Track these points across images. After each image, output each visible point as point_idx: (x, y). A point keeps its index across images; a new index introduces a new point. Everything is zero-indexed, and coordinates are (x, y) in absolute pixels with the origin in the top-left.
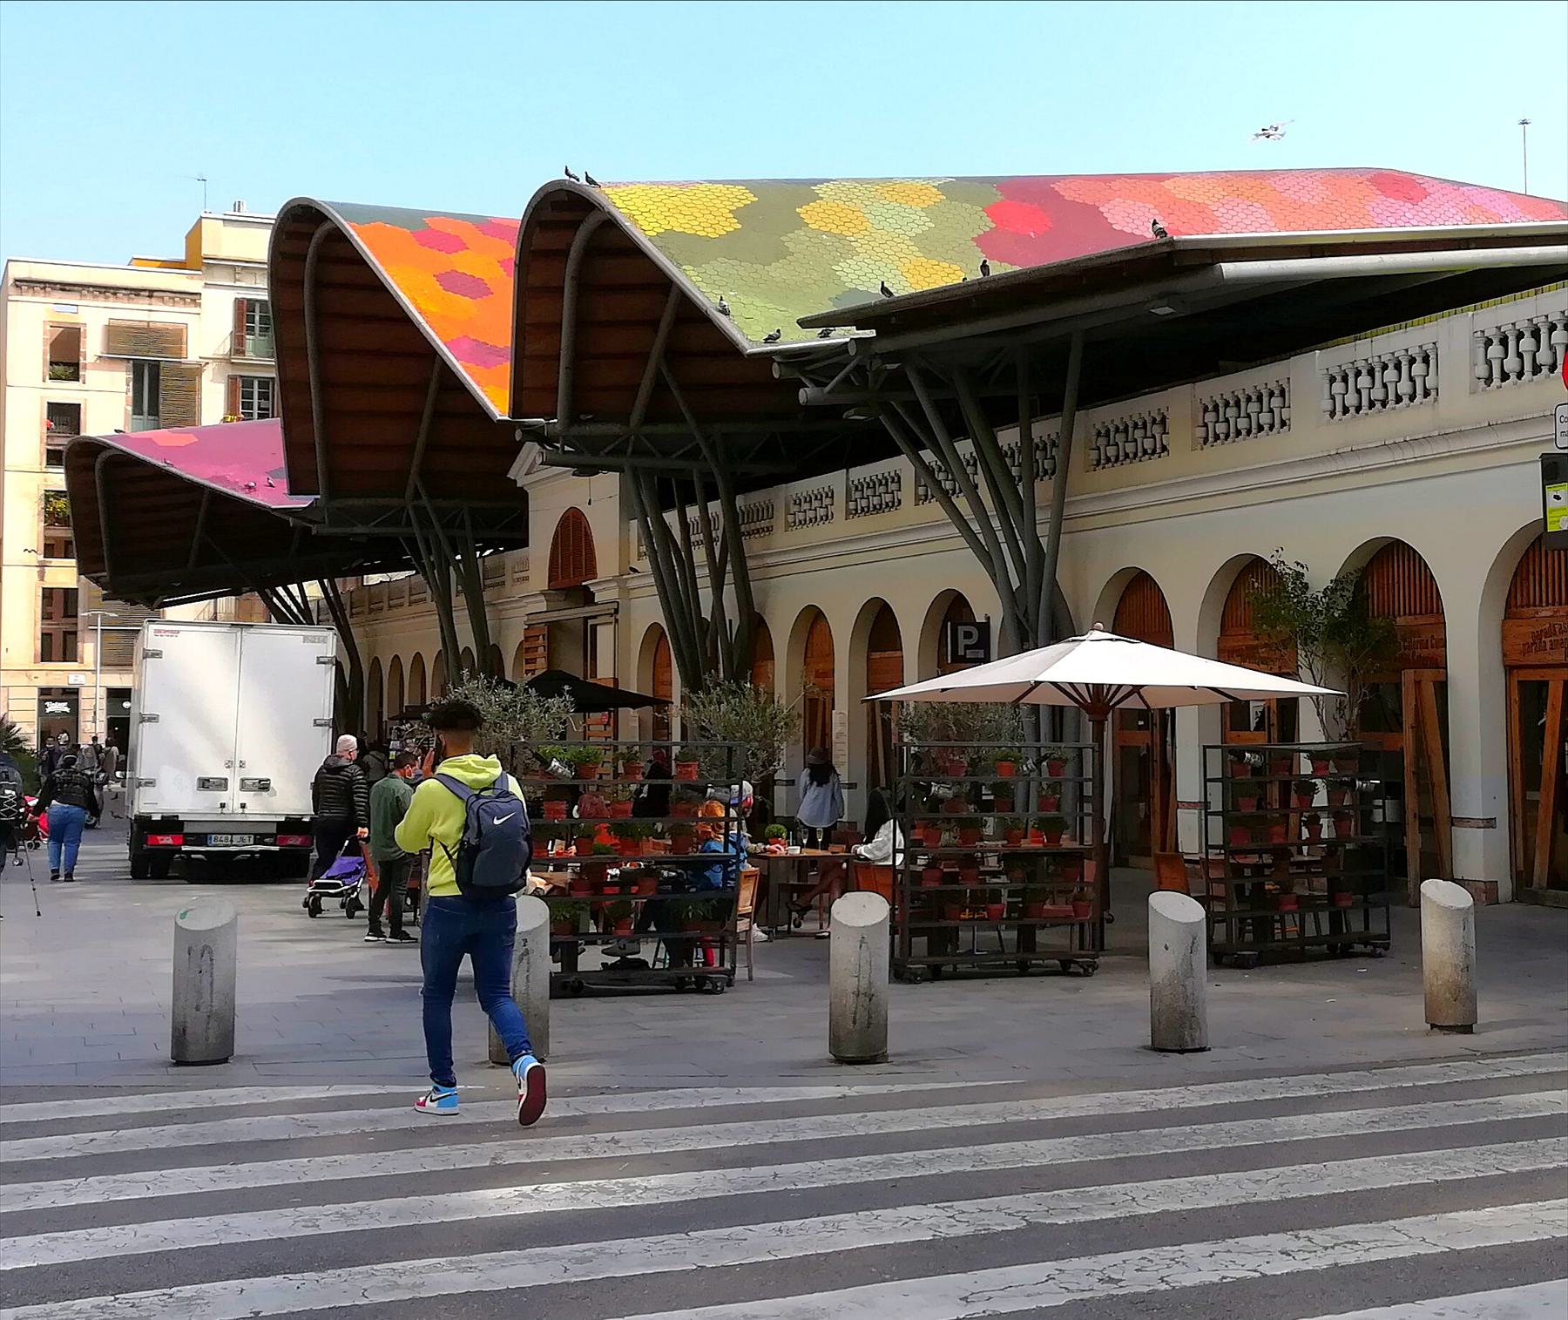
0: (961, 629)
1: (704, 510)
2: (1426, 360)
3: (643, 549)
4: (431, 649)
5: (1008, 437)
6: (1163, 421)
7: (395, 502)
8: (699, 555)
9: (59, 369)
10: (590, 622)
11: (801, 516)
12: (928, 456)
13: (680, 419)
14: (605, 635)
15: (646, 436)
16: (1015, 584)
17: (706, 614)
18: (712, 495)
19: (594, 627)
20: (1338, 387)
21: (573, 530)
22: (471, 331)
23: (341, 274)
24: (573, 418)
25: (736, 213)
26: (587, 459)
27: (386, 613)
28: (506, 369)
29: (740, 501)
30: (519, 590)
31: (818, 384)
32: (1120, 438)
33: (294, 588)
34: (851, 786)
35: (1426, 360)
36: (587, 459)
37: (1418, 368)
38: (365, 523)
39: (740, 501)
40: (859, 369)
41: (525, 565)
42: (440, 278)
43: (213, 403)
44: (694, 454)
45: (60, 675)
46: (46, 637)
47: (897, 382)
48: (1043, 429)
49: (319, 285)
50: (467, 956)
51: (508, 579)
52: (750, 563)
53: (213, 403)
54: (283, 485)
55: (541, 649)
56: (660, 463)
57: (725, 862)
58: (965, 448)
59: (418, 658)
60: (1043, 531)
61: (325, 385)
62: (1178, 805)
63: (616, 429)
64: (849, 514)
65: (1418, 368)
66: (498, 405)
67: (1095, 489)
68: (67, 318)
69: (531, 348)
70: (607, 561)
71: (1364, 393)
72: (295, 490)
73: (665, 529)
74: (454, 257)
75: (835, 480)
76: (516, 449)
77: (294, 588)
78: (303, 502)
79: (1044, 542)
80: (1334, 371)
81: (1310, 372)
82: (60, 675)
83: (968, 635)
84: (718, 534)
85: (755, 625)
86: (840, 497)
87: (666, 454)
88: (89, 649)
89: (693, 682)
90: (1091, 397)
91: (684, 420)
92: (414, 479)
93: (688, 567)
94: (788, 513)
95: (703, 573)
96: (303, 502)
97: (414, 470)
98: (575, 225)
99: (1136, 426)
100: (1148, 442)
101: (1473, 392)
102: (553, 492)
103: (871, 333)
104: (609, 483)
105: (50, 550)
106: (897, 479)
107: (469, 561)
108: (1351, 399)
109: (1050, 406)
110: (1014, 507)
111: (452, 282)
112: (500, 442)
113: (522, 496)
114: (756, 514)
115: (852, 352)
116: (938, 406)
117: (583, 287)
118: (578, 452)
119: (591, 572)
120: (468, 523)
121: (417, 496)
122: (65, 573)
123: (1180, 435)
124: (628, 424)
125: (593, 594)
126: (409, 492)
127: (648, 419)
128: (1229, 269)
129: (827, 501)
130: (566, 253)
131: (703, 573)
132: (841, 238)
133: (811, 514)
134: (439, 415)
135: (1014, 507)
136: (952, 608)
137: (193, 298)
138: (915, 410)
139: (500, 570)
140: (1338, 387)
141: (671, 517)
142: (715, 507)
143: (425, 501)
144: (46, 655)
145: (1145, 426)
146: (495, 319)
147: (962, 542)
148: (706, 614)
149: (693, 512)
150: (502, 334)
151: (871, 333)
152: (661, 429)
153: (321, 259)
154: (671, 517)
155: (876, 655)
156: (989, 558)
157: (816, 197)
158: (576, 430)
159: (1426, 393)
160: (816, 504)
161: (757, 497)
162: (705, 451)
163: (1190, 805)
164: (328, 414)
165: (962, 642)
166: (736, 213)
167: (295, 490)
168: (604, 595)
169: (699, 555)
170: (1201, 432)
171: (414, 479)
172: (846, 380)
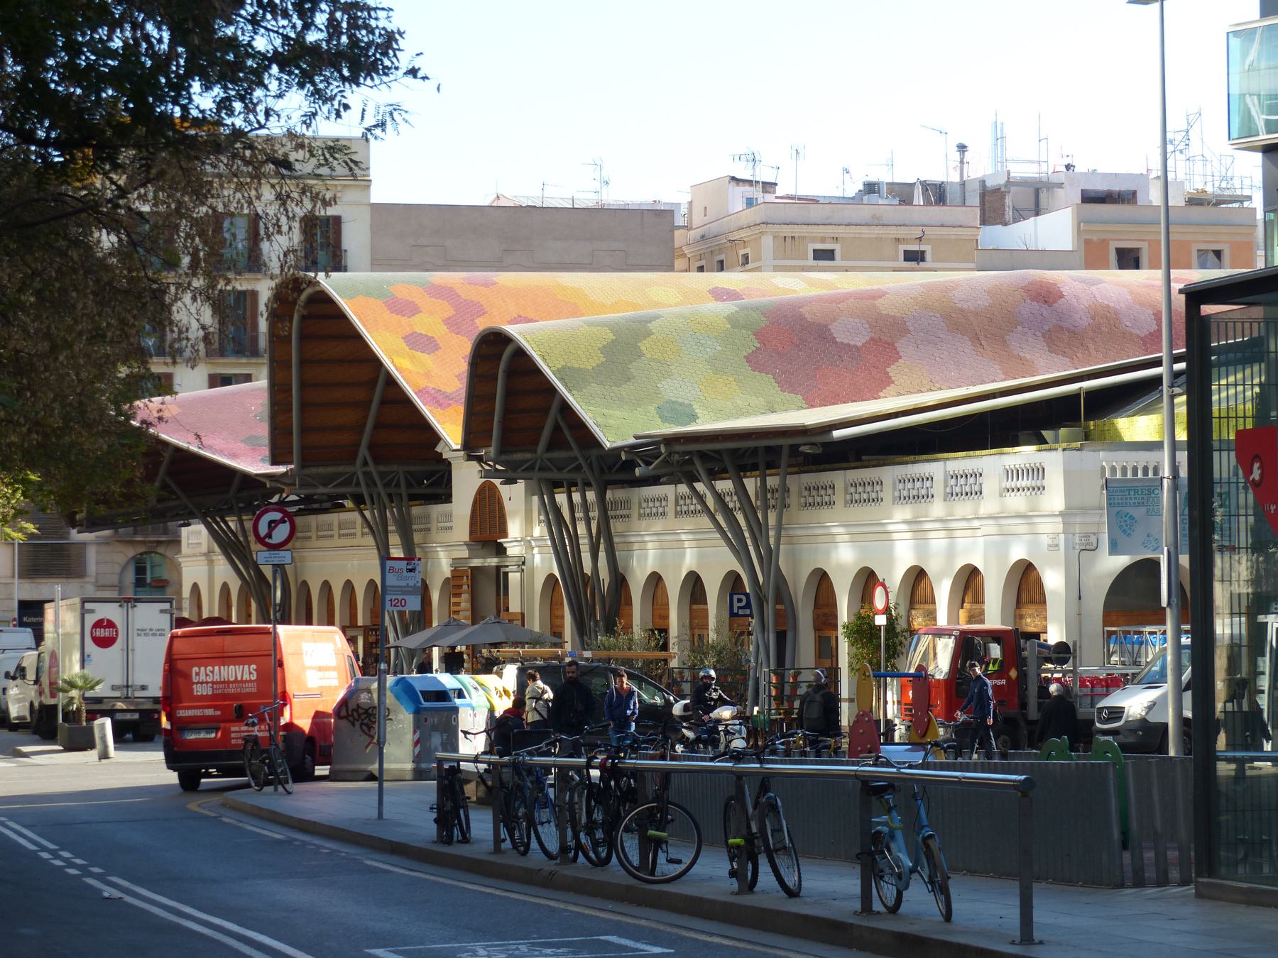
0: (736, 597)
3: (542, 518)
5: (751, 484)
7: (350, 469)
8: (581, 529)
10: (503, 570)
18: (587, 485)
26: (510, 474)
27: (314, 543)
31: (648, 464)
36: (510, 474)
38: (325, 485)
39: (609, 495)
41: (449, 516)
42: (407, 339)
44: (578, 469)
48: (772, 481)
51: (434, 526)
52: (616, 540)
55: (465, 587)
59: (349, 586)
60: (772, 541)
63: (528, 456)
64: (678, 514)
66: (450, 430)
67: (802, 520)
70: (515, 528)
73: (557, 511)
74: (416, 319)
78: (281, 469)
83: (740, 601)
85: (620, 581)
87: (560, 469)
92: (363, 451)
93: (575, 539)
94: (640, 507)
95: (584, 543)
96: (281, 469)
102: (467, 479)
106: (666, 499)
119: (504, 533)
120: (403, 483)
121: (365, 464)
124: (535, 452)
125: (505, 549)
126: (359, 461)
127: (551, 446)
128: (837, 434)
129: (664, 503)
131: (584, 543)
133: (654, 510)
134: (384, 402)
136: (733, 581)
139: (426, 518)
143: (371, 467)
147: (722, 542)
154: (561, 498)
155: (695, 607)
158: (503, 457)
160: (657, 504)
162: (585, 468)
163: (845, 700)
165: (736, 605)
167: (275, 462)
168: (513, 550)
169: (581, 529)
171: (363, 451)
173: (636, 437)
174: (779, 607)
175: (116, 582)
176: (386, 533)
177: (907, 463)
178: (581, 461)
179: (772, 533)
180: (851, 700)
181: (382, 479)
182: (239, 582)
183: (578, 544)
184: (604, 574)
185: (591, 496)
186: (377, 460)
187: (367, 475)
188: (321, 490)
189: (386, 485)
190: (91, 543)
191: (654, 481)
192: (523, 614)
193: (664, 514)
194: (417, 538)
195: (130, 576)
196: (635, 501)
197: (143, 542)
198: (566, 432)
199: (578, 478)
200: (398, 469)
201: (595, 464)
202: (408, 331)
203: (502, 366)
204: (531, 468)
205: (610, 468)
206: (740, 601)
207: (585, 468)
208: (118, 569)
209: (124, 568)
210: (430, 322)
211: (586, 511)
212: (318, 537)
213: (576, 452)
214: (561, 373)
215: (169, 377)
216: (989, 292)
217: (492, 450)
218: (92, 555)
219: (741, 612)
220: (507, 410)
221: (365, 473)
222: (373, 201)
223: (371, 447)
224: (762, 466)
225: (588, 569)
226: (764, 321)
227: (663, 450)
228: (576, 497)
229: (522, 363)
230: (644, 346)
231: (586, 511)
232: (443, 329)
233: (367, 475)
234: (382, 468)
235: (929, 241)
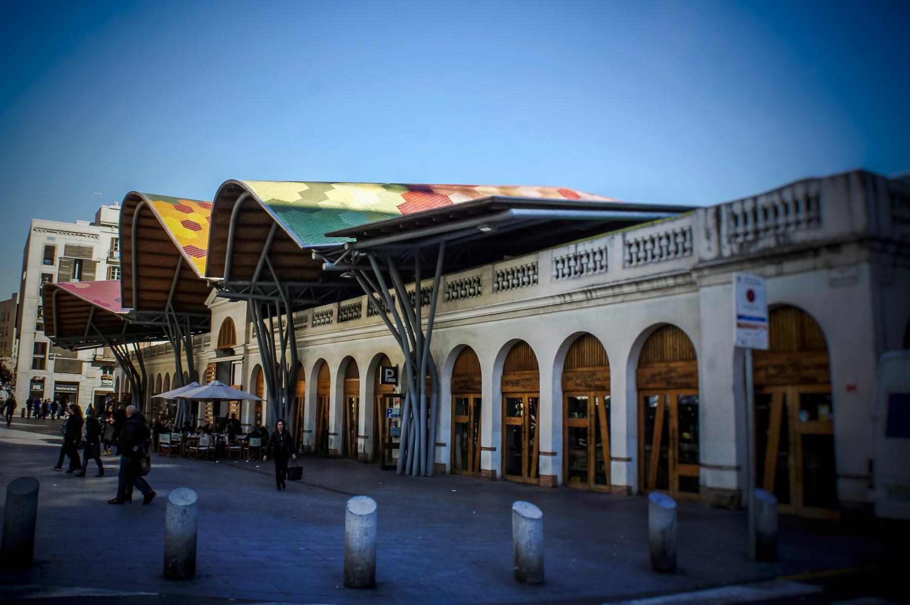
0: (387, 371)
1: (280, 319)
2: (601, 253)
4: (172, 372)
5: (411, 288)
6: (479, 281)
7: (161, 313)
8: (277, 336)
9: (47, 261)
11: (318, 321)
12: (377, 295)
13: (272, 280)
15: (259, 287)
16: (411, 349)
17: (279, 361)
20: (560, 266)
21: (228, 324)
22: (191, 236)
23: (145, 213)
24: (231, 277)
25: (301, 193)
26: (235, 295)
28: (204, 259)
29: (294, 315)
30: (207, 349)
31: (332, 262)
32: (459, 289)
33: (123, 346)
34: (335, 434)
35: (601, 253)
36: (235, 295)
37: (598, 257)
38: (150, 320)
39: (294, 315)
40: (349, 257)
43: (101, 274)
44: (277, 294)
45: (39, 374)
46: (35, 360)
47: (364, 262)
48: (426, 284)
49: (138, 226)
53: (101, 274)
56: (263, 297)
58: (392, 292)
59: (167, 375)
61: (138, 266)
62: (481, 449)
63: (246, 283)
65: (598, 257)
66: (199, 266)
68: (51, 243)
69: (216, 249)
70: (240, 338)
71: (572, 269)
72: (124, 306)
73: (264, 326)
75: (332, 307)
76: (207, 294)
77: (123, 346)
78: (126, 311)
79: (425, 333)
80: (558, 259)
81: (546, 260)
82: (39, 374)
83: (390, 373)
84: (284, 328)
85: (298, 365)
86: (335, 314)
87: (266, 294)
88: (50, 364)
90: (446, 271)
91: (273, 280)
92: (169, 304)
93: (272, 341)
94: (313, 320)
95: (278, 343)
96: (126, 311)
98: (235, 199)
99: (466, 283)
100: (473, 289)
101: (624, 267)
103: (355, 240)
104: (242, 306)
105: (39, 327)
106: (331, 313)
107: (189, 339)
108: (566, 271)
109: (428, 273)
110: (413, 318)
111: (187, 224)
112: (202, 289)
113: (209, 312)
114: (303, 319)
115: (346, 247)
116: (382, 272)
117: (237, 225)
118: (231, 292)
119: (234, 343)
121: (170, 310)
122: (42, 337)
123: (487, 289)
124: (251, 280)
127: (261, 278)
128: (515, 212)
130: (231, 211)
131: (278, 343)
134: (180, 279)
135: (413, 318)
136: (381, 360)
137: (96, 236)
138: (371, 274)
140: (560, 266)
141: (267, 321)
142: (284, 318)
143: (173, 313)
144: (34, 367)
145: (470, 283)
146: (201, 239)
148: (279, 361)
149: (275, 319)
151: (355, 240)
153: (140, 216)
154: (267, 321)
156: (400, 338)
158: (232, 283)
159: (602, 267)
161: (302, 314)
162: (281, 294)
163: (361, 437)
164: (138, 277)
165: (387, 376)
166: (301, 193)
167: (124, 306)
170: (496, 285)
171: (169, 304)
172: (342, 260)
174: (428, 377)
178: (279, 288)
179: (425, 321)
180: (366, 437)
183: (274, 346)
184: (289, 360)
186: (175, 310)
187: (170, 316)
188: (147, 323)
189: (180, 323)
194: (194, 351)
196: (310, 317)
198: (271, 269)
200: (187, 316)
202: (185, 219)
203: (232, 217)
204: (247, 292)
205: (296, 295)
206: (390, 373)
207: (281, 294)
213: (277, 283)
219: (390, 380)
220: (234, 252)
223: (173, 302)
224: (417, 275)
233: (170, 316)
234: (179, 314)
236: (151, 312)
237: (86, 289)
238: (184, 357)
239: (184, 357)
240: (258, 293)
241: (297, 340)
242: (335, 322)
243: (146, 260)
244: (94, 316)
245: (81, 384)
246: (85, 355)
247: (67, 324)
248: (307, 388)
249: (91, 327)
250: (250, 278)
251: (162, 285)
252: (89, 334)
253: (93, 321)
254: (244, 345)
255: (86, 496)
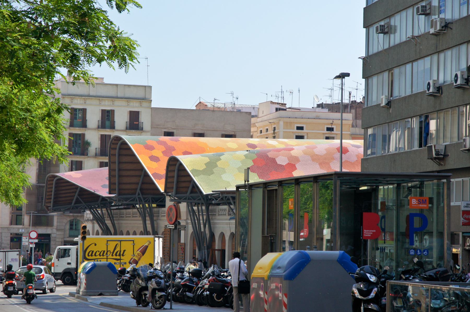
8: (201, 218)
14: (183, 232)
19: (180, 231)
23: (124, 147)
28: (163, 180)
36: (179, 201)
38: (126, 201)
39: (210, 207)
44: (200, 199)
50: (360, 189)
54: (107, 190)
57: (41, 93)
66: (162, 190)
73: (193, 210)
85: (212, 235)
87: (194, 199)
89: (200, 250)
93: (199, 220)
97: (139, 189)
102: (169, 203)
111: (154, 159)
121: (139, 194)
127: (192, 192)
132: (224, 169)
139: (158, 212)
141: (195, 208)
143: (141, 196)
150: (163, 172)
152: (193, 195)
157: (220, 159)
167: (110, 193)
169: (201, 218)
171: (138, 191)
173: (213, 191)
175: (63, 228)
176: (145, 217)
177: (394, 193)
181: (144, 199)
182: (192, 230)
185: (204, 208)
186: (143, 194)
190: (56, 215)
191: (218, 204)
192: (185, 244)
193: (225, 214)
194: (155, 218)
195: (68, 227)
196: (217, 210)
197: (73, 216)
199: (200, 202)
201: (205, 199)
208: (64, 224)
209: (66, 224)
210: (157, 153)
211: (202, 213)
212: (126, 217)
214: (193, 171)
215: (81, 162)
216: (326, 150)
217: (174, 193)
218: (55, 219)
221: (139, 198)
222: (152, 107)
223: (141, 189)
225: (202, 230)
226: (255, 157)
227: (221, 195)
228: (200, 208)
229: (181, 168)
230: (218, 163)
231: (202, 213)
232: (162, 155)
235: (335, 124)
236: (125, 196)
237: (80, 178)
238: (148, 222)
239: (148, 222)
240: (191, 199)
241: (211, 221)
242: (227, 215)
243: (124, 166)
244: (80, 191)
245: (53, 236)
246: (55, 216)
247: (61, 197)
248: (217, 246)
249: (77, 199)
250: (186, 192)
251: (134, 180)
252: (75, 204)
253: (79, 195)
254: (185, 220)
255: (338, 199)
